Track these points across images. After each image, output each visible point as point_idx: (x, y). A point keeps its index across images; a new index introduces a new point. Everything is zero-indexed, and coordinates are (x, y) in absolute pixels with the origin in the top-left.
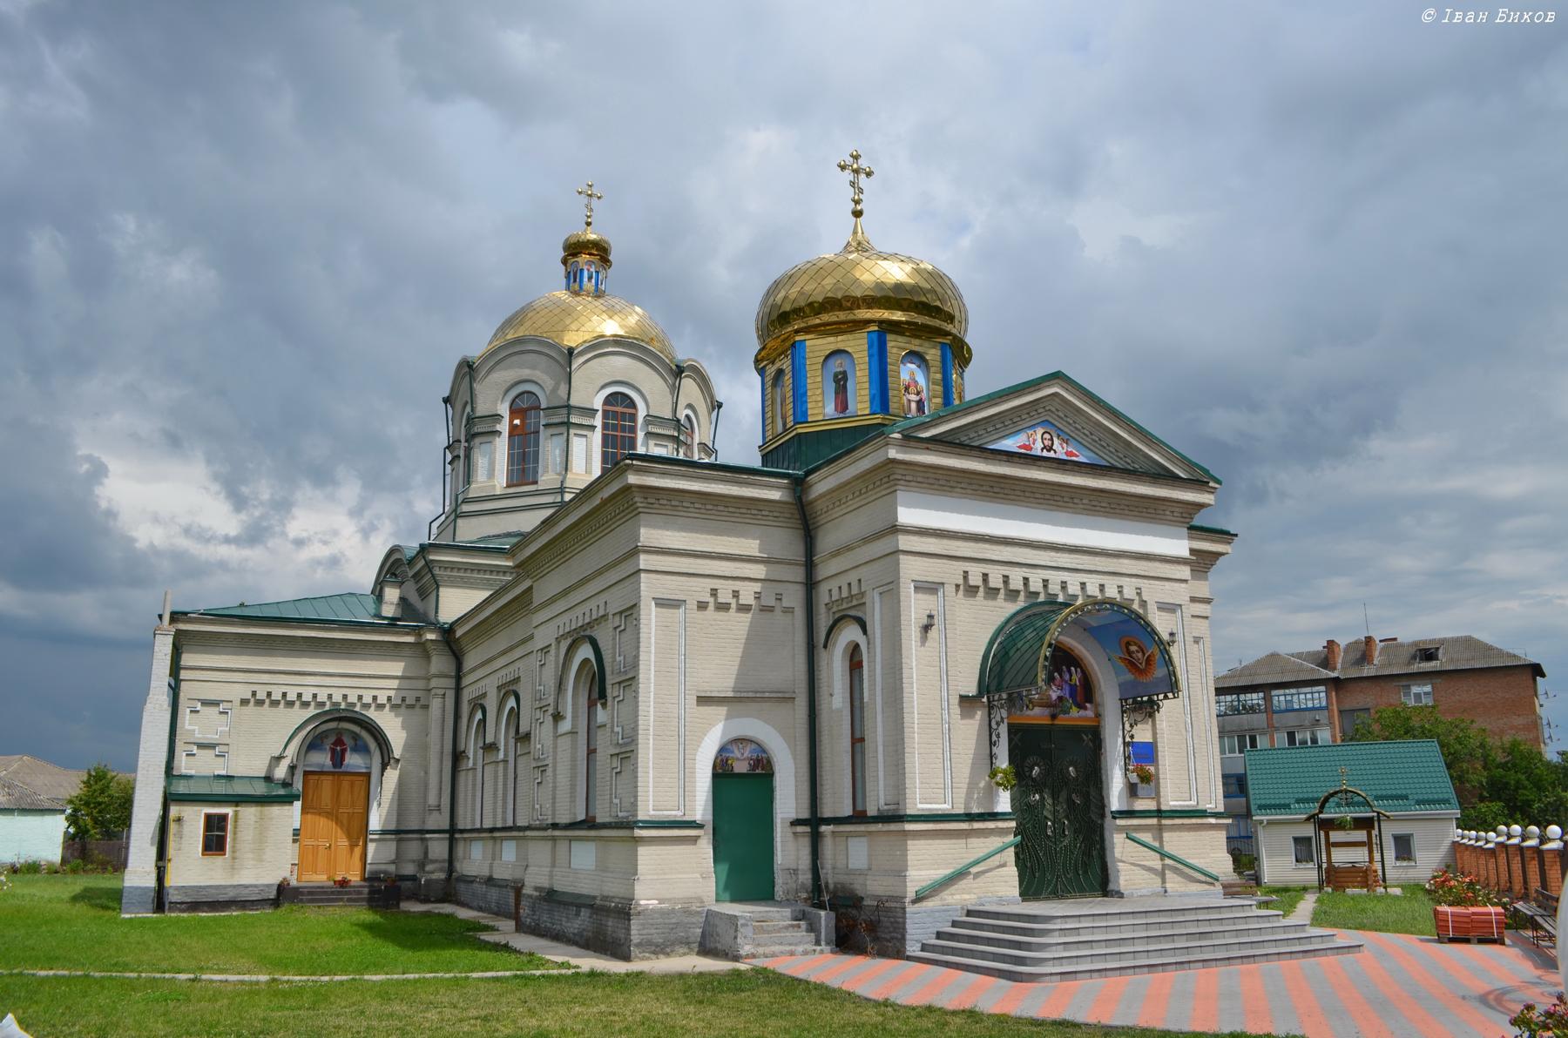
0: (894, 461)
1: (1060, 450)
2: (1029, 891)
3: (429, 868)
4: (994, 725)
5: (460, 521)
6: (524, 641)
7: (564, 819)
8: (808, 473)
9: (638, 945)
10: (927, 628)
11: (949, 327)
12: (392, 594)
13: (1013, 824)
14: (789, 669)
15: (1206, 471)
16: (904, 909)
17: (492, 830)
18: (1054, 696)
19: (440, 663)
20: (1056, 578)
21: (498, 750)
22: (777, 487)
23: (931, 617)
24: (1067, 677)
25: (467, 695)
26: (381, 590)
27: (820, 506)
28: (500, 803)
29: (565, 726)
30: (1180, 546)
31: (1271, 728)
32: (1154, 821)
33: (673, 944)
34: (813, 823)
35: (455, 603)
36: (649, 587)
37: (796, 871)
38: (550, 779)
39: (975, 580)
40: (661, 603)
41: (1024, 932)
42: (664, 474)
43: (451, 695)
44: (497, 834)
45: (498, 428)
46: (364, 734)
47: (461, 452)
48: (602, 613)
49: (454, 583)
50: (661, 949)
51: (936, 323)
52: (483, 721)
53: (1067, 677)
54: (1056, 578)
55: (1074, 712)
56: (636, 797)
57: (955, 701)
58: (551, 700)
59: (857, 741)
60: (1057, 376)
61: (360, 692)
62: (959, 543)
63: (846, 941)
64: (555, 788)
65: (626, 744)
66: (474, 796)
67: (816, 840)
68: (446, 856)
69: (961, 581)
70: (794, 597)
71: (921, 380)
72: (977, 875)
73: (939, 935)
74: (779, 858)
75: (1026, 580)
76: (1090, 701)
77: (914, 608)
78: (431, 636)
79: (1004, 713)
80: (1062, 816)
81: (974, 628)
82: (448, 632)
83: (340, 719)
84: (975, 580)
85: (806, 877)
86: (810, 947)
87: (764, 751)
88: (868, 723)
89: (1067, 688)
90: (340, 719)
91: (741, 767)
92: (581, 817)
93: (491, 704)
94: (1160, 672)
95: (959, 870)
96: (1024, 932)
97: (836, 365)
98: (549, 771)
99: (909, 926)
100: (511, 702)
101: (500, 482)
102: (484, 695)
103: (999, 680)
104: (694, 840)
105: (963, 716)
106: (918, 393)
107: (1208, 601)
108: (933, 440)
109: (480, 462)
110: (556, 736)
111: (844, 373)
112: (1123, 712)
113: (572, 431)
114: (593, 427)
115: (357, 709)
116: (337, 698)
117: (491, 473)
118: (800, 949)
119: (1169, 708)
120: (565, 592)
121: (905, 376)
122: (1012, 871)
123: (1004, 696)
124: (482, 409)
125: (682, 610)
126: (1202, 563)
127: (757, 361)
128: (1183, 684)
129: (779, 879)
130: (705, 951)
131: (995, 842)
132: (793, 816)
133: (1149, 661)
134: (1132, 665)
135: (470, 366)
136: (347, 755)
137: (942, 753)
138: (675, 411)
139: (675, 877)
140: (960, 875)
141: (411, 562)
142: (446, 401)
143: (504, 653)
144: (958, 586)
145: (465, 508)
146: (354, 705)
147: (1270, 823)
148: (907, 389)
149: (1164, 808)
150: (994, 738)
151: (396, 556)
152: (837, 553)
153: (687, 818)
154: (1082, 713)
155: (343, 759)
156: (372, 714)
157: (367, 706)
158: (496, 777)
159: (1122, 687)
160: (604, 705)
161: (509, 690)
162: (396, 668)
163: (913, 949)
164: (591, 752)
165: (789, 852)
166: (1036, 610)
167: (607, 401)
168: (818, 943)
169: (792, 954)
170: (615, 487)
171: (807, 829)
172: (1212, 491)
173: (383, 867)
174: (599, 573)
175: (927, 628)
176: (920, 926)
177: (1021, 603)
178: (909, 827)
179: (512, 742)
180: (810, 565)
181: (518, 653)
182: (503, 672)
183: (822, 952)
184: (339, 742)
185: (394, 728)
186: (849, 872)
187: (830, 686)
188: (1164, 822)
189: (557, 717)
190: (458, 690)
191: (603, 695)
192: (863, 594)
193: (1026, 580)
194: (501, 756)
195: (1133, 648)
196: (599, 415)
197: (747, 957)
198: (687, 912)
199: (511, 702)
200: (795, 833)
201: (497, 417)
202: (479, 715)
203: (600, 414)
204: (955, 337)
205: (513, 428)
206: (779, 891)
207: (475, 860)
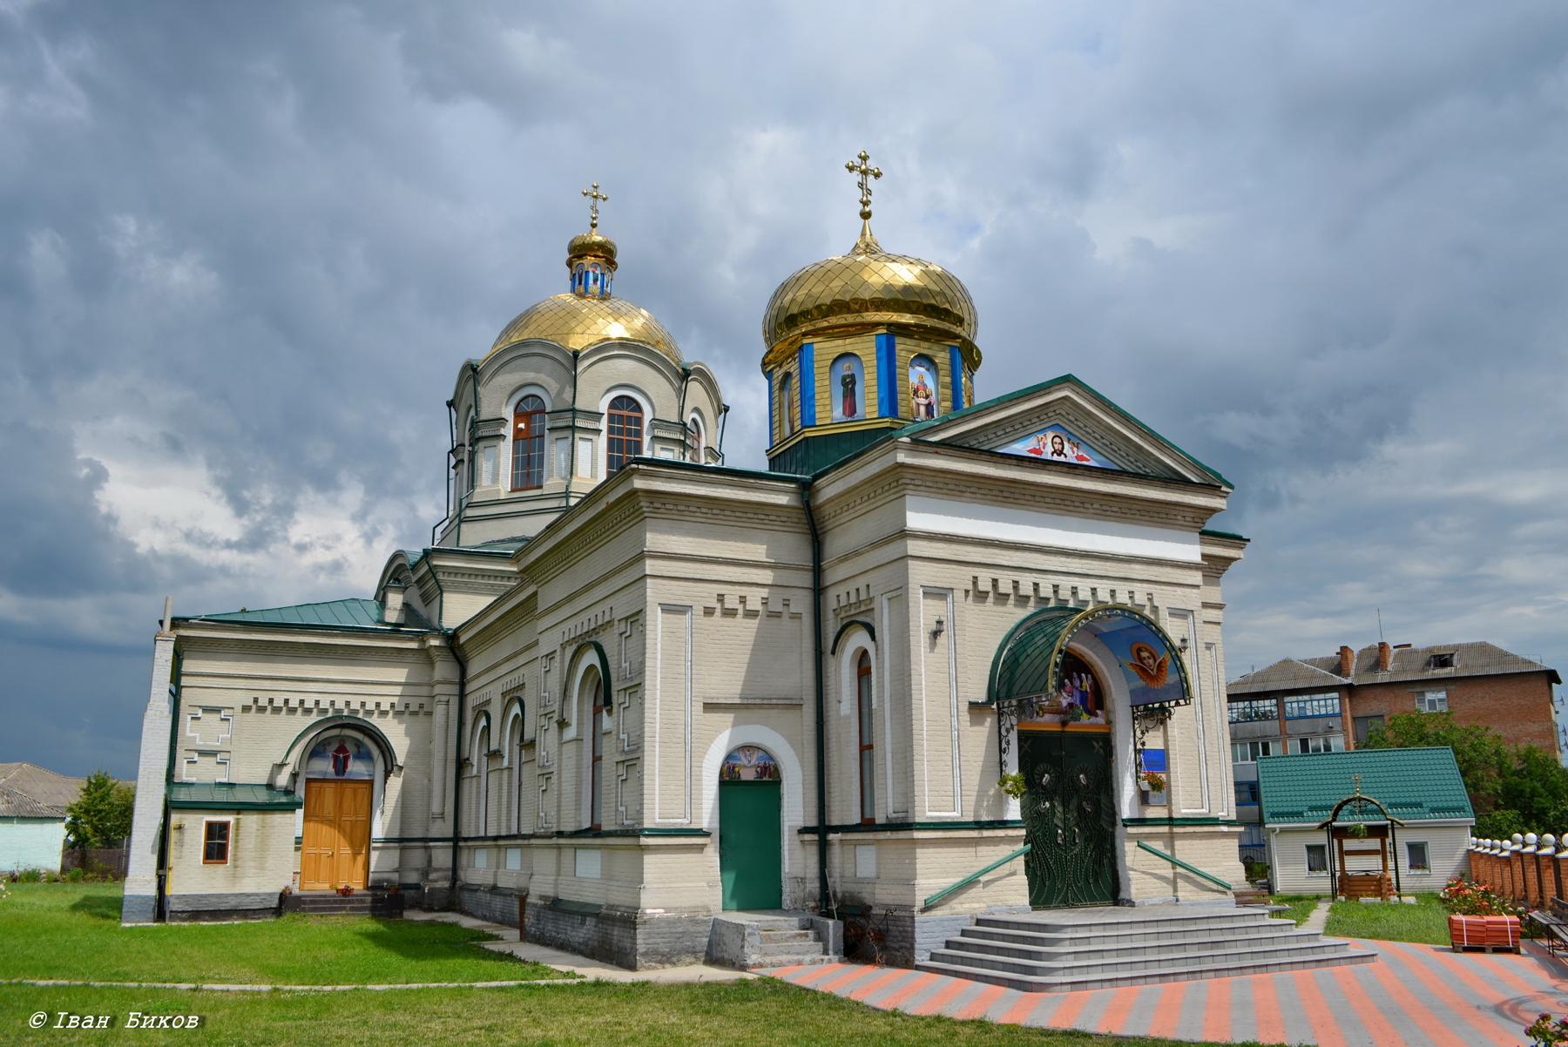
0: (902, 465)
1: (1070, 454)
2: (1040, 898)
3: (433, 876)
6: (528, 648)
8: (816, 477)
9: (644, 954)
10: (936, 634)
11: (958, 330)
12: (395, 600)
13: (1023, 832)
14: (796, 676)
15: (1218, 476)
16: (913, 917)
17: (496, 838)
18: (1065, 703)
19: (444, 669)
20: (1066, 583)
21: (502, 757)
22: (785, 492)
23: (940, 622)
25: (471, 701)
27: (828, 510)
28: (504, 811)
29: (571, 733)
30: (1191, 551)
31: (1284, 736)
32: (1166, 829)
33: (679, 953)
34: (821, 831)
36: (655, 592)
37: (803, 879)
39: (985, 585)
40: (668, 609)
41: (1034, 941)
42: (670, 478)
43: (454, 701)
45: (502, 431)
46: (367, 741)
47: (464, 457)
48: (607, 618)
49: (458, 589)
50: (667, 959)
52: (488, 727)
53: (1077, 683)
54: (1066, 583)
55: (1085, 719)
57: (964, 707)
58: (556, 707)
59: (866, 748)
60: (1068, 380)
61: (363, 699)
63: (854, 951)
64: (560, 795)
65: (632, 751)
66: (478, 803)
67: (823, 848)
68: (450, 864)
69: (970, 587)
75: (1036, 585)
76: (1101, 708)
77: (923, 613)
78: (434, 642)
81: (983, 634)
82: (451, 638)
84: (985, 585)
85: (813, 886)
86: (818, 957)
87: (771, 758)
91: (748, 775)
92: (587, 825)
93: (495, 710)
94: (1171, 678)
95: (968, 878)
96: (1034, 941)
97: (844, 368)
98: (554, 778)
100: (516, 709)
101: (504, 487)
102: (488, 702)
103: (1010, 687)
105: (973, 723)
106: (927, 397)
107: (1220, 607)
109: (484, 466)
110: (561, 744)
111: (853, 376)
113: (577, 435)
114: (598, 431)
115: (360, 716)
116: (340, 704)
117: (495, 477)
119: (1180, 715)
120: (570, 598)
121: (914, 380)
122: (1022, 880)
123: (1014, 702)
124: (486, 413)
125: (688, 615)
126: (1214, 568)
128: (1195, 690)
130: (712, 960)
131: (1005, 850)
132: (800, 824)
134: (1143, 671)
135: (474, 369)
136: (351, 763)
137: (952, 761)
139: (681, 885)
141: (415, 567)
142: (450, 404)
143: (508, 659)
144: (967, 591)
145: (469, 513)
146: (357, 711)
147: (1283, 831)
148: (916, 392)
149: (1175, 816)
150: (1004, 745)
152: (845, 558)
153: (693, 826)
154: (1093, 720)
155: (345, 766)
156: (375, 720)
157: (370, 713)
158: (500, 785)
160: (610, 712)
161: (514, 696)
162: (399, 674)
163: (921, 958)
164: (597, 759)
165: (797, 860)
166: (1045, 616)
167: (613, 405)
168: (826, 952)
169: (800, 963)
170: (620, 491)
171: (815, 837)
172: (1224, 495)
173: (386, 876)
175: (936, 634)
176: (929, 936)
177: (1031, 609)
179: (516, 749)
180: (817, 571)
181: (522, 660)
183: (830, 961)
185: (397, 735)
187: (839, 693)
188: (1176, 830)
189: (562, 724)
190: (462, 696)
191: (608, 702)
192: (871, 600)
193: (1036, 585)
194: (506, 763)
195: (1145, 654)
197: (754, 966)
199: (516, 709)
201: (501, 421)
204: (964, 340)
205: (517, 431)
206: (787, 900)
207: (479, 868)
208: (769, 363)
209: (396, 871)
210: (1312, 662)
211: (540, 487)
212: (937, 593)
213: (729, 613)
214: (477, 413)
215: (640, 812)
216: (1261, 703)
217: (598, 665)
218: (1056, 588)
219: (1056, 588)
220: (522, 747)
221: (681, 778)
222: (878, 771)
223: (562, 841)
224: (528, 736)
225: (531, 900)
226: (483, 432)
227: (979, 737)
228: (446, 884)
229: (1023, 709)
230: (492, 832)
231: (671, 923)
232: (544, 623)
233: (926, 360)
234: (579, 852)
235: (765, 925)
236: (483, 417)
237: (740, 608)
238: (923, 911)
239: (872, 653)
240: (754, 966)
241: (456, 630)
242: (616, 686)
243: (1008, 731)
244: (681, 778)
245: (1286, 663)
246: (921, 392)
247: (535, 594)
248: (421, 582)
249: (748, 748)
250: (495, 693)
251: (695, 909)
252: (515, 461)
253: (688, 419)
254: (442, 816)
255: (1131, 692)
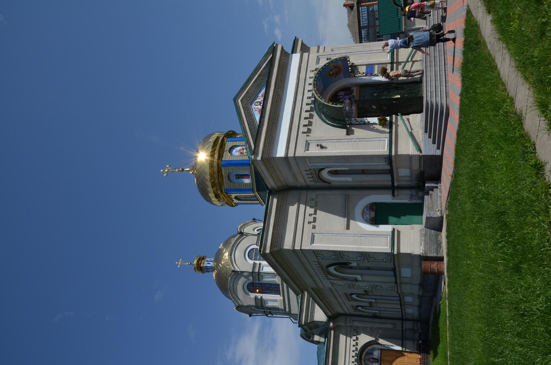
0: (262, 158)
1: (260, 99)
2: (420, 111)
3: (416, 329)
4: (358, 123)
5: (292, 312)
6: (331, 291)
7: (393, 279)
8: (268, 189)
9: (437, 254)
10: (322, 147)
11: (221, 138)
12: (316, 338)
13: (394, 116)
14: (336, 197)
15: (270, 47)
16: (424, 156)
17: (401, 305)
18: (348, 101)
19: (341, 322)
20: (306, 101)
21: (371, 302)
22: (273, 199)
23: (318, 145)
24: (341, 97)
25: (353, 312)
26: (316, 341)
27: (279, 184)
28: (391, 302)
29: (359, 277)
30: (296, 58)
31: (375, 26)
32: (395, 65)
33: (437, 241)
34: (393, 189)
35: (320, 316)
36: (307, 246)
37: (411, 195)
38: (379, 284)
39: (305, 129)
40: (312, 242)
41: (432, 112)
42: (266, 240)
43: (353, 318)
44: (402, 303)
45: (259, 297)
46: (366, 350)
47: (270, 312)
48: (317, 263)
49: (312, 316)
50: (439, 245)
51: (220, 140)
52: (362, 307)
53: (341, 97)
54: (306, 101)
55: (354, 94)
56: (382, 253)
57: (348, 137)
58: (350, 282)
59: (363, 172)
60: (235, 100)
61: (351, 351)
62: (292, 135)
63: (437, 178)
64: (382, 282)
65: (364, 256)
66: (389, 311)
67: (400, 188)
68: (411, 322)
69: (306, 134)
70: (312, 194)
71: (239, 148)
72: (412, 129)
73: (434, 143)
74: (406, 201)
75: (306, 111)
76: (351, 88)
77: (314, 151)
78: (331, 324)
79: (353, 119)
80: (394, 98)
81: (322, 130)
82: (331, 318)
83: (361, 359)
84: (305, 129)
85: (414, 192)
86: (439, 190)
87: (367, 206)
88: (356, 168)
89: (345, 97)
90: (361, 359)
91: (373, 214)
92: (392, 273)
93: (355, 304)
94: (340, 63)
95: (410, 136)
96: (432, 112)
97: (233, 178)
98: (376, 284)
99: (431, 153)
100: (354, 296)
101: (279, 297)
102: (352, 306)
103: (340, 120)
104: (399, 232)
105: (353, 134)
106: (243, 149)
107: (319, 47)
108: (255, 144)
109: (270, 304)
110: (363, 281)
111: (236, 175)
112: (355, 76)
113: (261, 271)
114: (260, 264)
115: (357, 352)
116: (353, 360)
117: (276, 301)
118: (439, 194)
119: (353, 60)
120: (311, 276)
121: (238, 154)
122: (411, 117)
123: (347, 119)
124: (253, 303)
125: (315, 235)
126: (305, 49)
127: (232, 206)
128: (344, 55)
129: (414, 201)
130: (440, 230)
131: (400, 122)
132: (391, 196)
133: (336, 67)
134: (337, 73)
135: (238, 307)
136: (374, 357)
137: (368, 142)
138: (255, 235)
139: (412, 239)
140: (411, 135)
141: (305, 330)
142: (250, 316)
143: (336, 299)
144: (307, 136)
145: (287, 310)
146: (356, 353)
147: (405, 25)
148: (242, 153)
149: (390, 61)
150: (362, 123)
151: (304, 335)
152: (296, 178)
153: (391, 234)
154: (355, 91)
155: (375, 359)
156: (359, 347)
157: (356, 349)
158: (382, 303)
159: (345, 77)
160: (350, 263)
161: (349, 297)
162: (342, 338)
163: (438, 153)
164: (368, 268)
165: (403, 198)
166: (317, 108)
167: (251, 259)
168: (437, 187)
169: (441, 197)
170: (271, 257)
171: (396, 191)
172: (277, 45)
173: (415, 346)
174: (303, 264)
175: (322, 147)
176: (430, 149)
177: (314, 113)
178: (393, 154)
179: (368, 297)
180: (301, 188)
181: (336, 294)
182: (344, 299)
183: (440, 186)
184: (369, 360)
185: (364, 339)
186: (411, 176)
187: (344, 182)
188: (395, 61)
189: (356, 280)
190: (351, 315)
191: (346, 264)
192: (310, 170)
193: (306, 111)
194: (374, 301)
195: (331, 73)
196: (256, 262)
197: (442, 213)
198: (425, 235)
199: (354, 296)
200: (397, 195)
201: (256, 298)
202: (360, 308)
203: (255, 262)
204: (224, 136)
205: (260, 292)
206: (419, 201)
207: (412, 311)
208: (232, 204)
209: (413, 342)
210: (349, 17)
211: (279, 285)
212: (307, 145)
213: (315, 220)
214: (253, 306)
215: (386, 253)
216: (363, 34)
217: (334, 267)
218: (307, 104)
219: (307, 104)
220: (367, 295)
221: (369, 238)
222: (372, 168)
223: (398, 282)
224: (363, 293)
225: (421, 293)
226: (259, 304)
227: (358, 132)
228: (419, 324)
229: (350, 117)
230: (399, 307)
231: (426, 244)
232: (321, 286)
233: (231, 150)
234: (402, 276)
235: (427, 210)
236: (254, 304)
237: (313, 216)
238: (421, 152)
239: (329, 169)
240: (442, 213)
241: (327, 316)
242: (341, 261)
243: (357, 121)
244: (369, 238)
245: (349, 26)
246: (242, 151)
247: (312, 288)
248: (311, 328)
249: (363, 214)
250: (349, 304)
251: (421, 235)
252: (269, 293)
253: (256, 232)
254: (394, 324)
255: (345, 78)
